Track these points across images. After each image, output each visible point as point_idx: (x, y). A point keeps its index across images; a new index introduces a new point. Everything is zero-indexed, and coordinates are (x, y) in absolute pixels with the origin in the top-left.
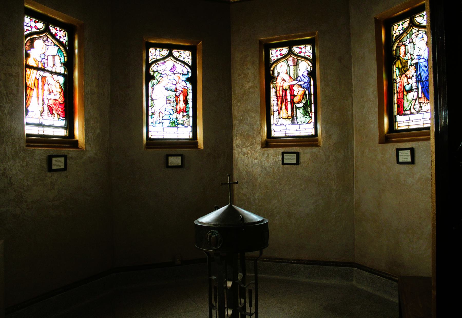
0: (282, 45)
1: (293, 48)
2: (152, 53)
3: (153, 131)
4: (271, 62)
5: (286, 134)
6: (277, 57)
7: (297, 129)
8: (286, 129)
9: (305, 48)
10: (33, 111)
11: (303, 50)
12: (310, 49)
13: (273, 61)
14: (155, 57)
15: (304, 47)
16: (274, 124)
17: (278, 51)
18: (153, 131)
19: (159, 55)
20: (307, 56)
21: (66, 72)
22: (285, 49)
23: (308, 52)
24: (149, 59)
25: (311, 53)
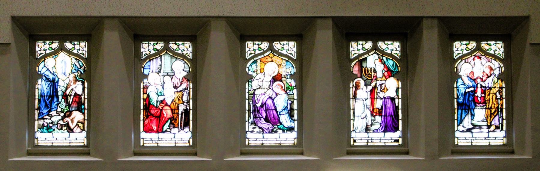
0: (52, 38)
1: (379, 43)
2: (458, 48)
3: (478, 137)
4: (143, 57)
5: (70, 143)
6: (46, 51)
7: (171, 139)
8: (263, 138)
9: (393, 45)
10: (362, 113)
11: (286, 47)
12: (501, 47)
13: (144, 56)
14: (460, 52)
15: (392, 44)
16: (457, 130)
17: (46, 44)
18: (478, 137)
19: (258, 49)
20: (290, 54)
21: (386, 69)
22: (264, 43)
23: (396, 50)
24: (350, 54)
25: (399, 52)
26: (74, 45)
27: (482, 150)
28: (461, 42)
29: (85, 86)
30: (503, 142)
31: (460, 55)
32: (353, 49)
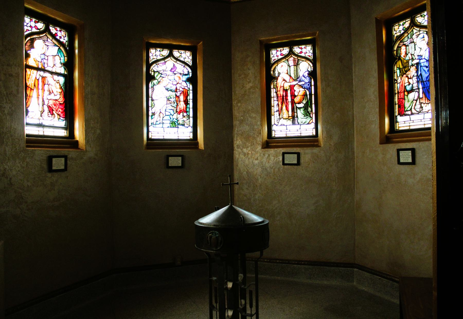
0: (282, 45)
1: (294, 48)
4: (272, 62)
5: (286, 134)
6: (278, 57)
7: (297, 130)
8: (287, 129)
9: (306, 48)
11: (304, 50)
12: (310, 49)
13: (273, 61)
15: (305, 48)
16: (274, 124)
17: (278, 51)
20: (308, 56)
22: (286, 49)
23: (309, 52)
25: (312, 53)
26: (301, 48)
27: (426, 133)
28: (276, 49)
29: (312, 84)
30: (190, 136)
31: (276, 60)
32: (273, 56)
